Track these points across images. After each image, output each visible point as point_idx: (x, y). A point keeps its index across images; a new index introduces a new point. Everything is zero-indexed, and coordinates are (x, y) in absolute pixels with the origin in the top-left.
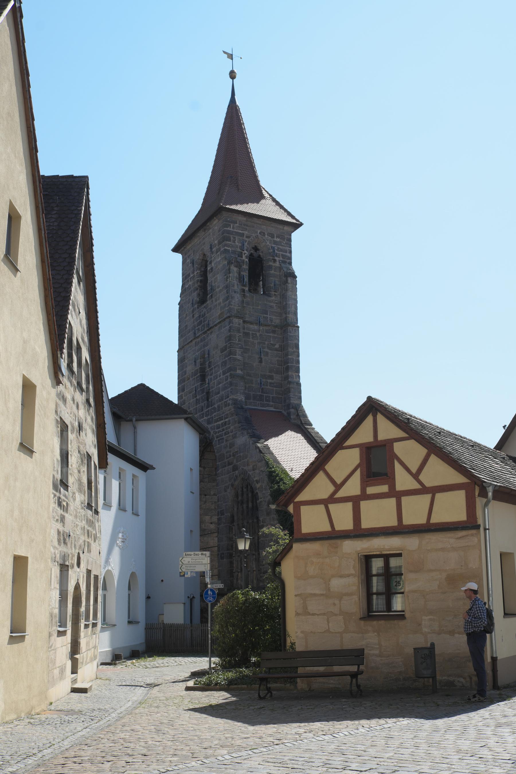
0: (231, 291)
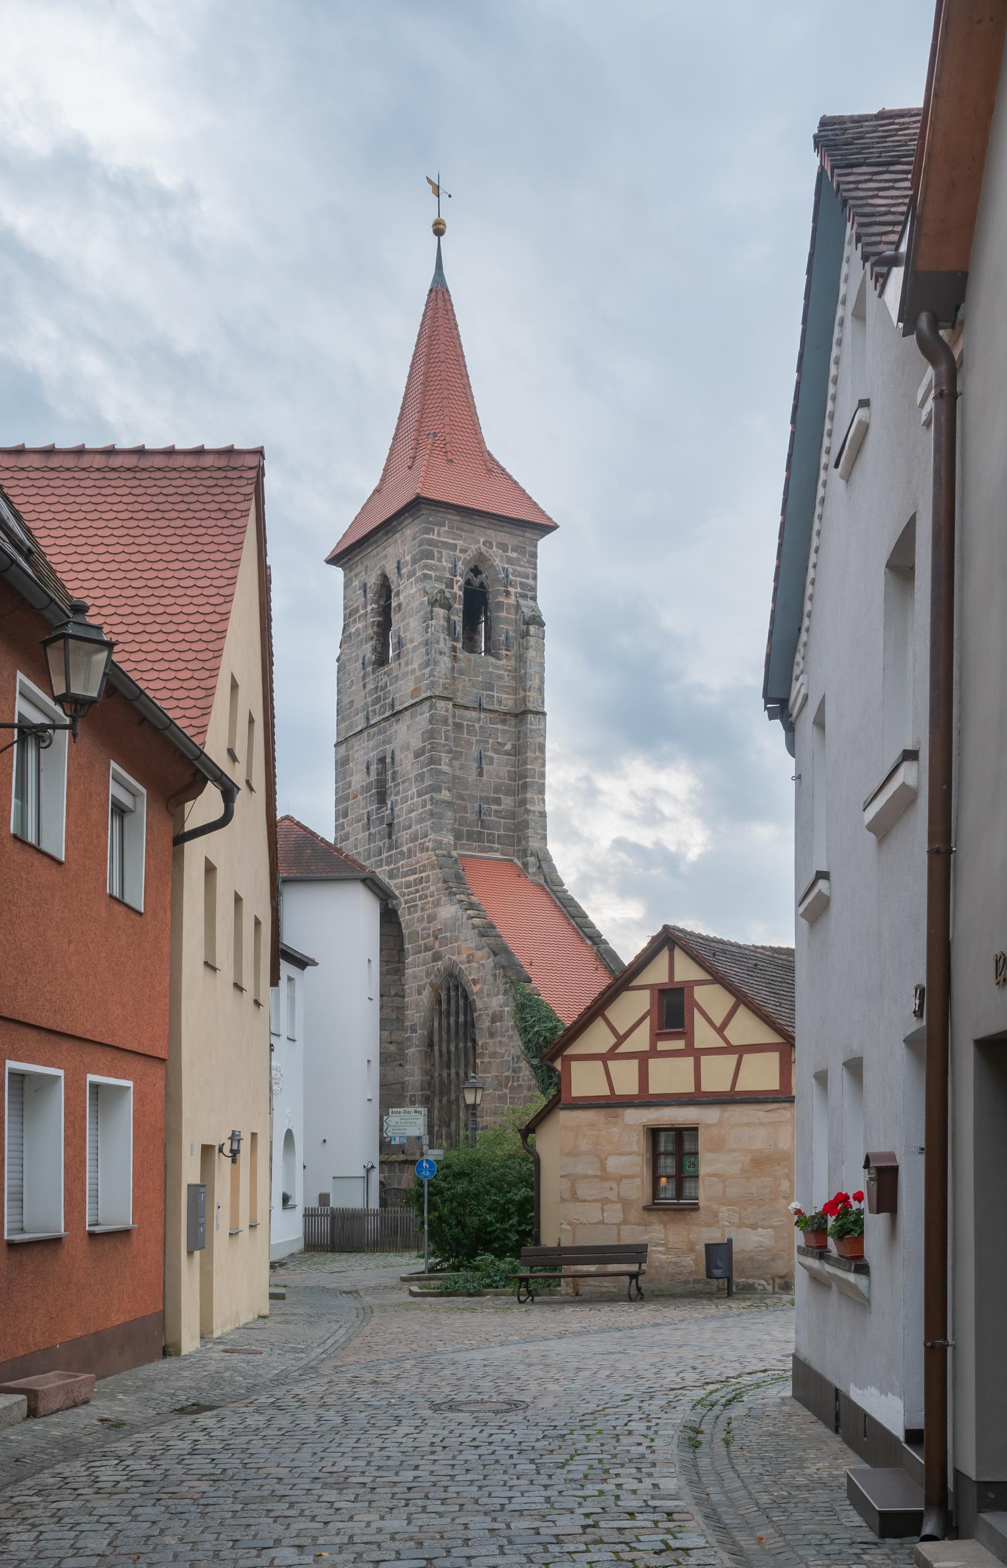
0: (433, 652)
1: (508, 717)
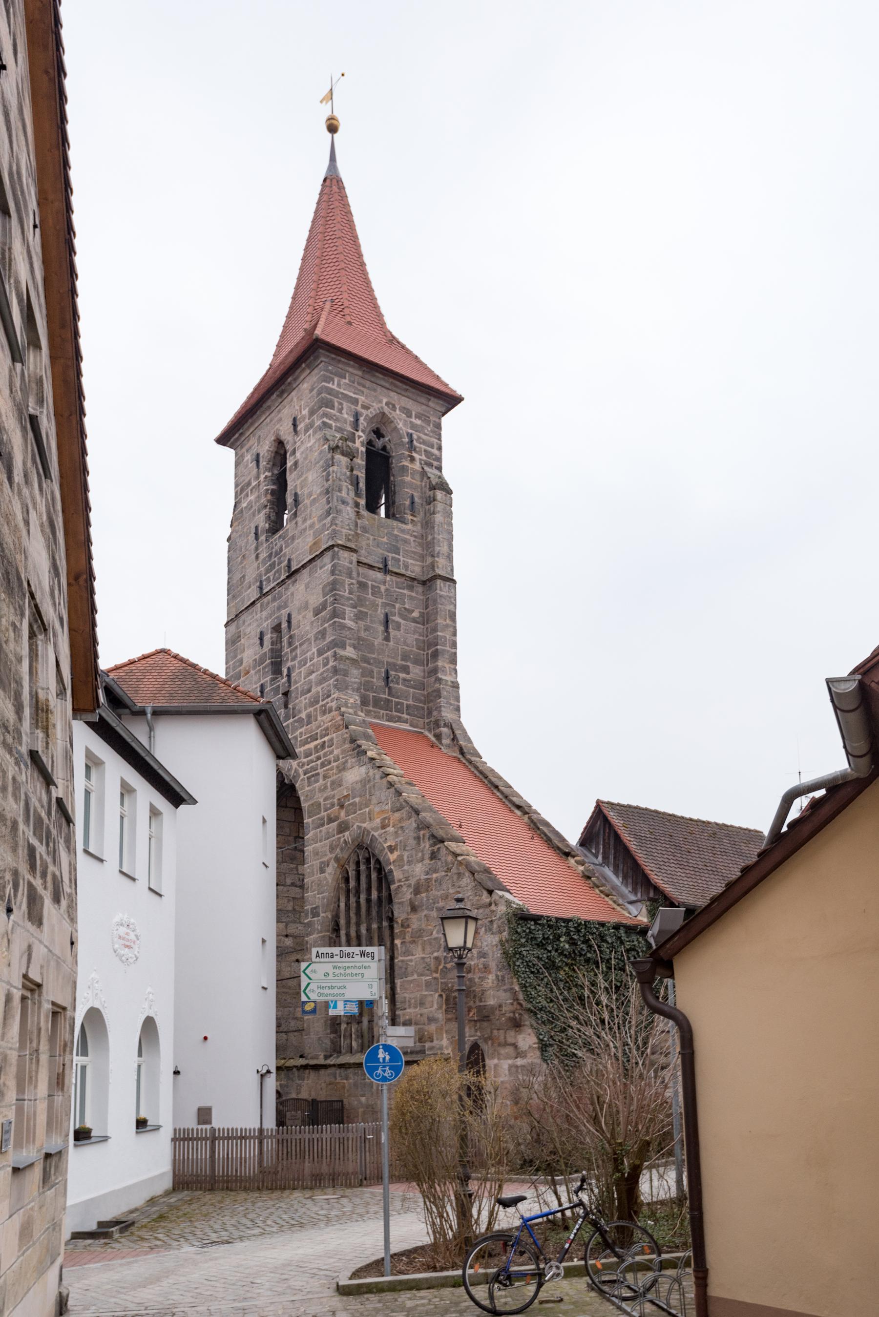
1: (415, 583)
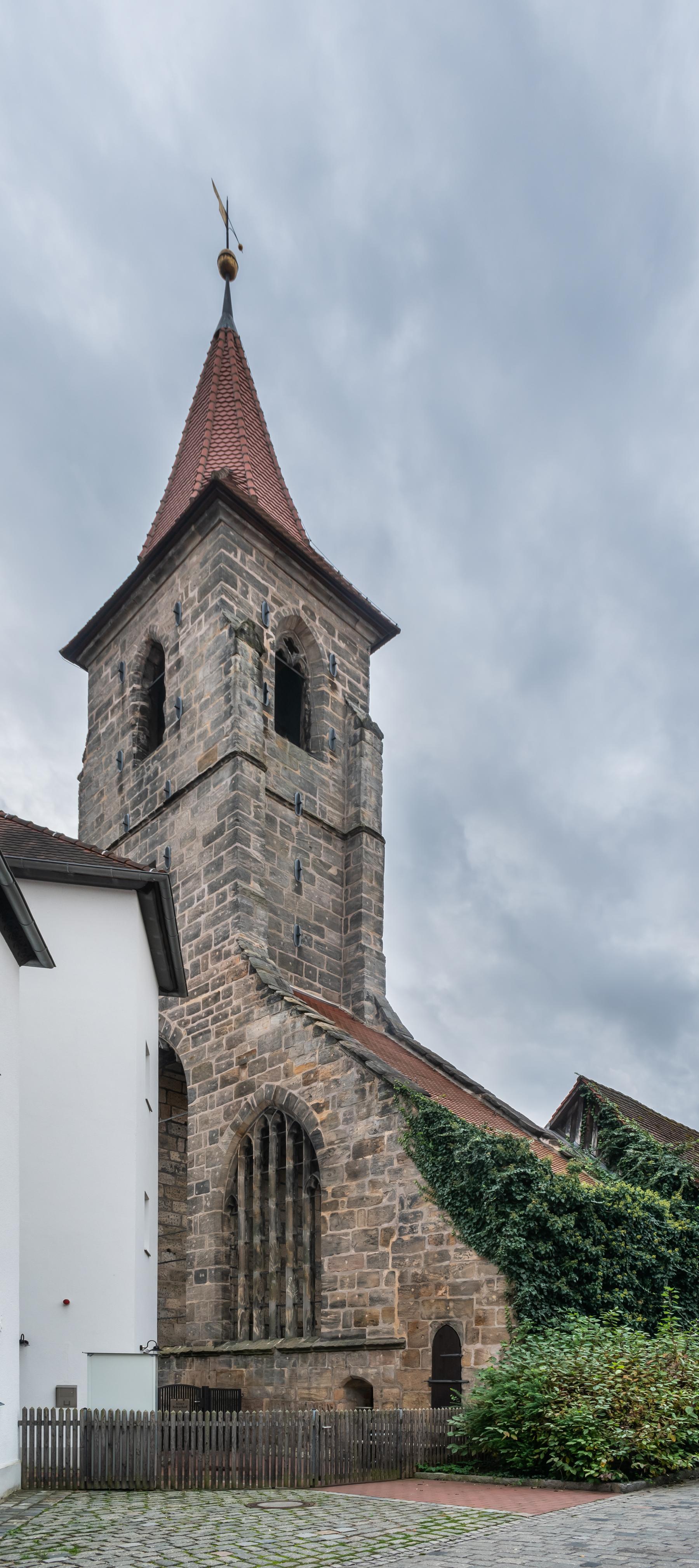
1: (333, 835)
